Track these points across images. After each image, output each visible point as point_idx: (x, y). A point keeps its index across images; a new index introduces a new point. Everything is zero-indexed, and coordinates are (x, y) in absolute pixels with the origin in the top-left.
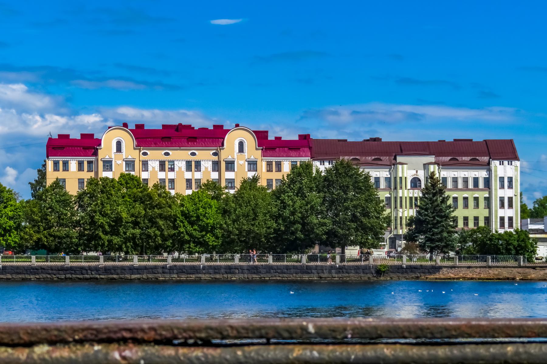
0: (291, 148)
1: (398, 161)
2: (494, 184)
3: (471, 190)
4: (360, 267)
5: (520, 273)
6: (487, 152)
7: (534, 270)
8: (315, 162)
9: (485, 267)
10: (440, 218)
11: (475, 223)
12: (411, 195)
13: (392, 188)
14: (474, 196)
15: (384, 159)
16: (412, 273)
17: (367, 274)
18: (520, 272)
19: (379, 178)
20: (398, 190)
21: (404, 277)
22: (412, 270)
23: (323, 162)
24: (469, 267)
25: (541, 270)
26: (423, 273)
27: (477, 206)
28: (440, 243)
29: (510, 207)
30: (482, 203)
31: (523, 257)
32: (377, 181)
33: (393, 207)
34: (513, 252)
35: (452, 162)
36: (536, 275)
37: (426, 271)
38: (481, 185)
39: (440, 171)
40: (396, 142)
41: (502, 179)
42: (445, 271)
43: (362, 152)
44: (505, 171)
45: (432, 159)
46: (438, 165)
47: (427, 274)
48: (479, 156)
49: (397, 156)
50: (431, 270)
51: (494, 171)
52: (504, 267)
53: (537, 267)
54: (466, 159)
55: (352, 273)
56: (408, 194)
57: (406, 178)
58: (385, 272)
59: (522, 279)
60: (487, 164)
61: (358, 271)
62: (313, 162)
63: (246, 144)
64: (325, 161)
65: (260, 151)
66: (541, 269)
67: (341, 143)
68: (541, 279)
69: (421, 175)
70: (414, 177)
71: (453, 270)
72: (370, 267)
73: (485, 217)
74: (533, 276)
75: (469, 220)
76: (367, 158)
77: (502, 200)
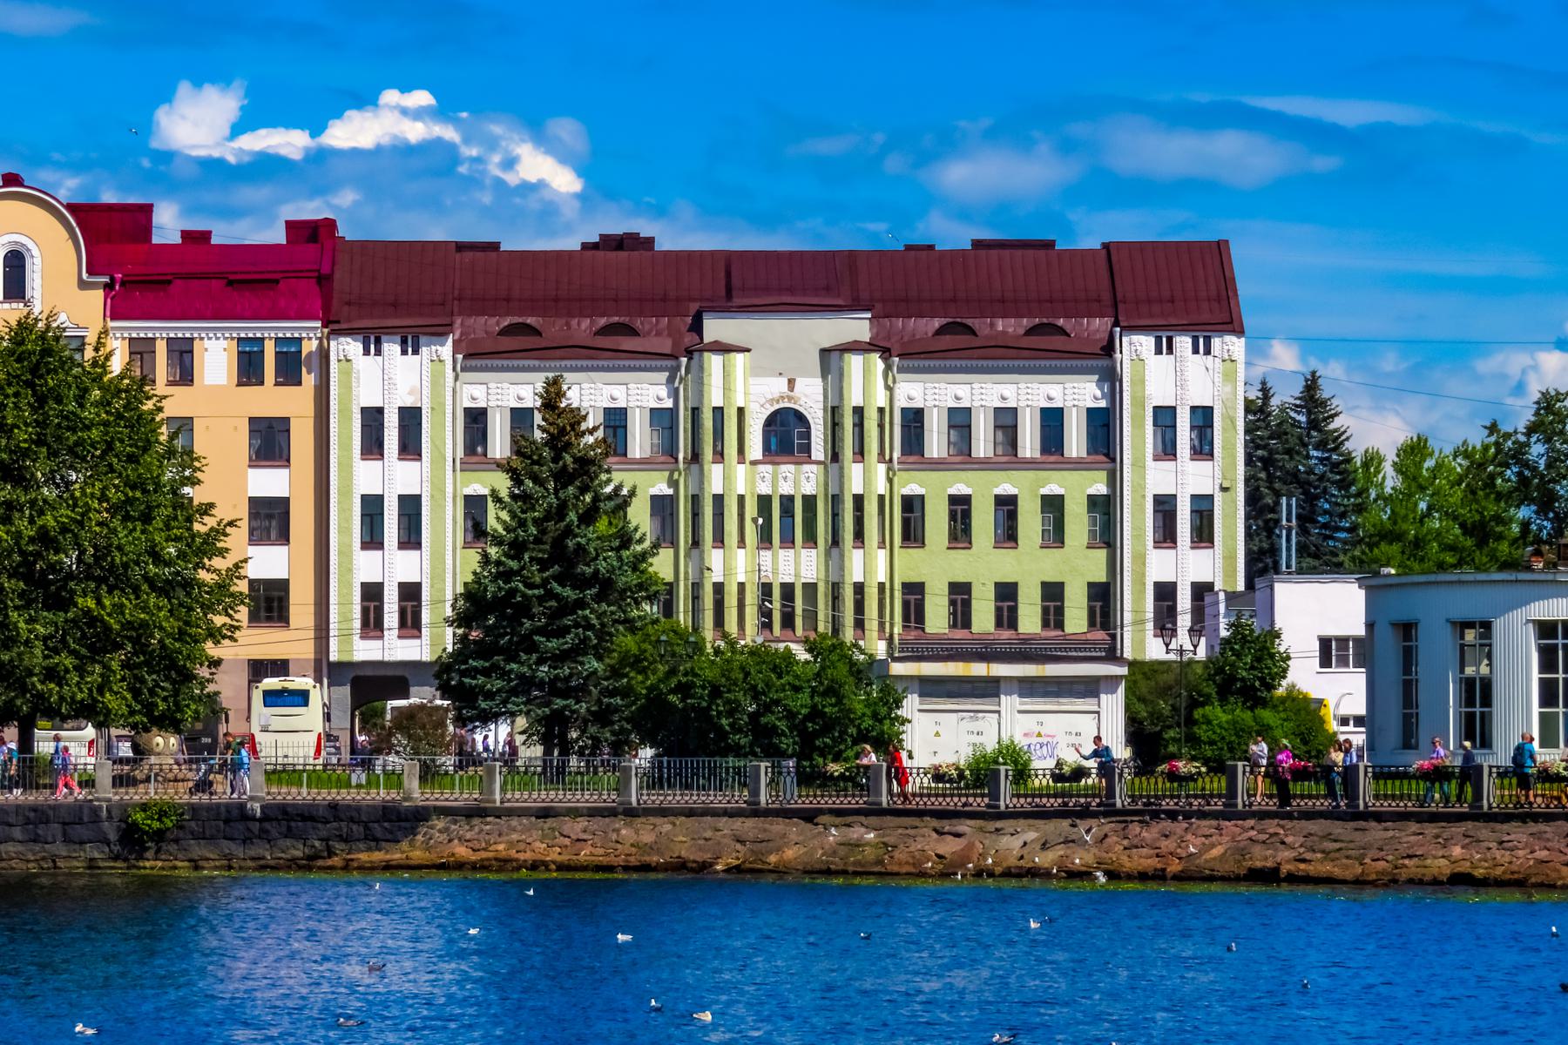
1: (708, 337)
2: (351, 438)
4: (51, 813)
5: (742, 842)
6: (1106, 296)
7: (809, 826)
8: (342, 339)
9: (611, 813)
10: (574, 588)
12: (765, 489)
13: (681, 456)
14: (1045, 491)
15: (647, 327)
16: (289, 842)
17: (82, 843)
18: (744, 838)
19: (1060, 411)
20: (706, 467)
21: (253, 859)
22: (289, 829)
23: (378, 342)
24: (545, 813)
27: (1055, 535)
28: (571, 702)
29: (1201, 541)
30: (1078, 522)
31: (773, 767)
33: (686, 542)
35: (947, 341)
38: (1075, 441)
39: (894, 382)
41: (1165, 417)
42: (440, 831)
43: (907, 300)
44: (1180, 382)
45: (857, 327)
46: (886, 353)
47: (361, 846)
49: (705, 316)
50: (377, 829)
52: (690, 813)
53: (821, 812)
55: (13, 840)
56: (751, 482)
57: (741, 411)
58: (169, 835)
59: (737, 869)
60: (1102, 349)
61: (40, 832)
62: (333, 343)
63: (37, 261)
64: (384, 338)
65: (100, 293)
67: (469, 255)
68: (817, 867)
69: (810, 398)
70: (777, 407)
72: (96, 811)
73: (1091, 585)
76: (574, 322)
77: (1165, 507)
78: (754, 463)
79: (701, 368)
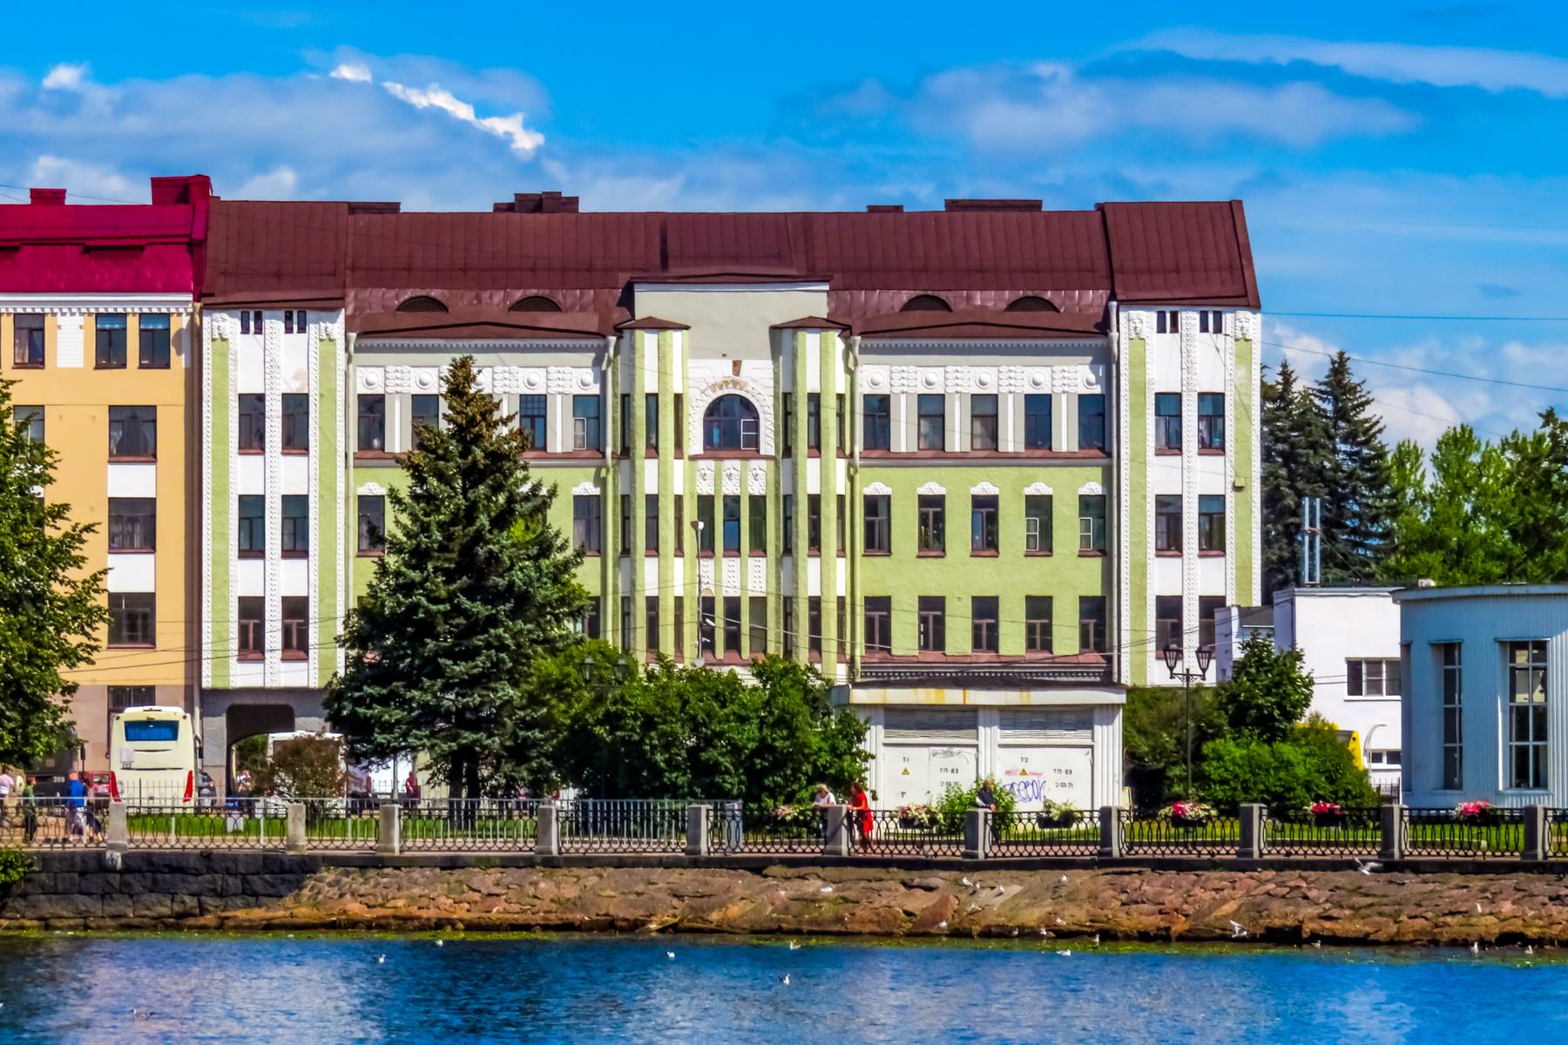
0: (97, 248)
1: (640, 313)
3: (1012, 460)
6: (1101, 263)
7: (758, 878)
8: (217, 315)
9: (528, 863)
10: (485, 602)
11: (1031, 630)
12: (706, 488)
13: (609, 451)
14: (1030, 491)
15: (569, 301)
16: (154, 897)
19: (941, 398)
20: (638, 463)
21: (113, 917)
22: (155, 881)
23: (258, 318)
25: (788, 879)
26: (220, 894)
27: (1042, 542)
28: (482, 735)
29: (1210, 548)
30: (1068, 527)
31: (715, 810)
32: (533, 418)
33: (615, 550)
34: (732, 782)
35: (917, 317)
36: (750, 906)
37: (234, 883)
38: (1065, 434)
39: (856, 364)
40: (646, 215)
41: (1169, 405)
42: (330, 885)
44: (1186, 366)
45: (813, 300)
46: (846, 331)
47: (239, 901)
48: (1056, 289)
49: (637, 288)
50: (257, 883)
51: (1132, 365)
52: (620, 863)
53: (770, 862)
54: (988, 300)
56: (690, 480)
57: (678, 398)
58: (15, 889)
60: (1097, 326)
64: (265, 313)
66: (791, 872)
67: (363, 218)
69: (759, 381)
70: (720, 393)
71: (366, 881)
73: (1083, 599)
74: (735, 910)
75: (1002, 616)
76: (486, 295)
77: (1169, 510)
78: (694, 458)
79: (632, 348)
